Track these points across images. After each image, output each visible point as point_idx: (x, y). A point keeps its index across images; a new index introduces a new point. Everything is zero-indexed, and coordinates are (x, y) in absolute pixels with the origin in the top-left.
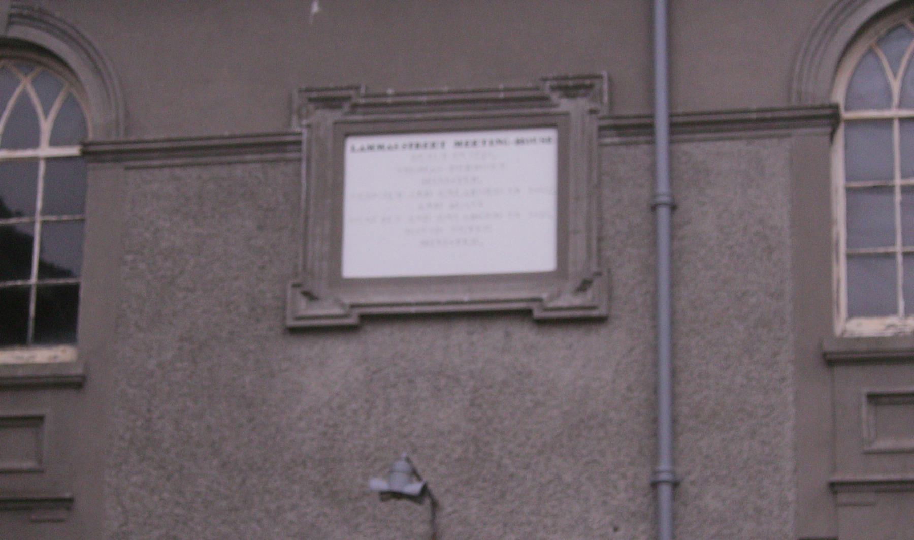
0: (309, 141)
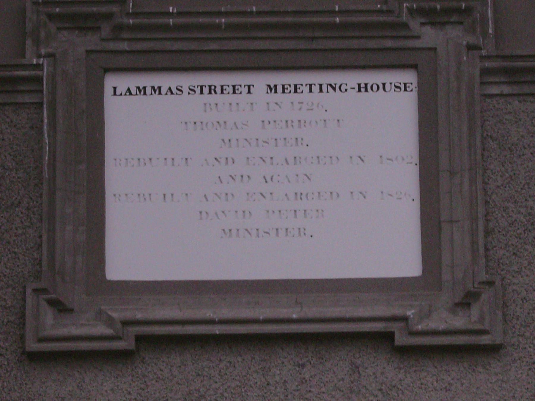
0: (53, 77)
